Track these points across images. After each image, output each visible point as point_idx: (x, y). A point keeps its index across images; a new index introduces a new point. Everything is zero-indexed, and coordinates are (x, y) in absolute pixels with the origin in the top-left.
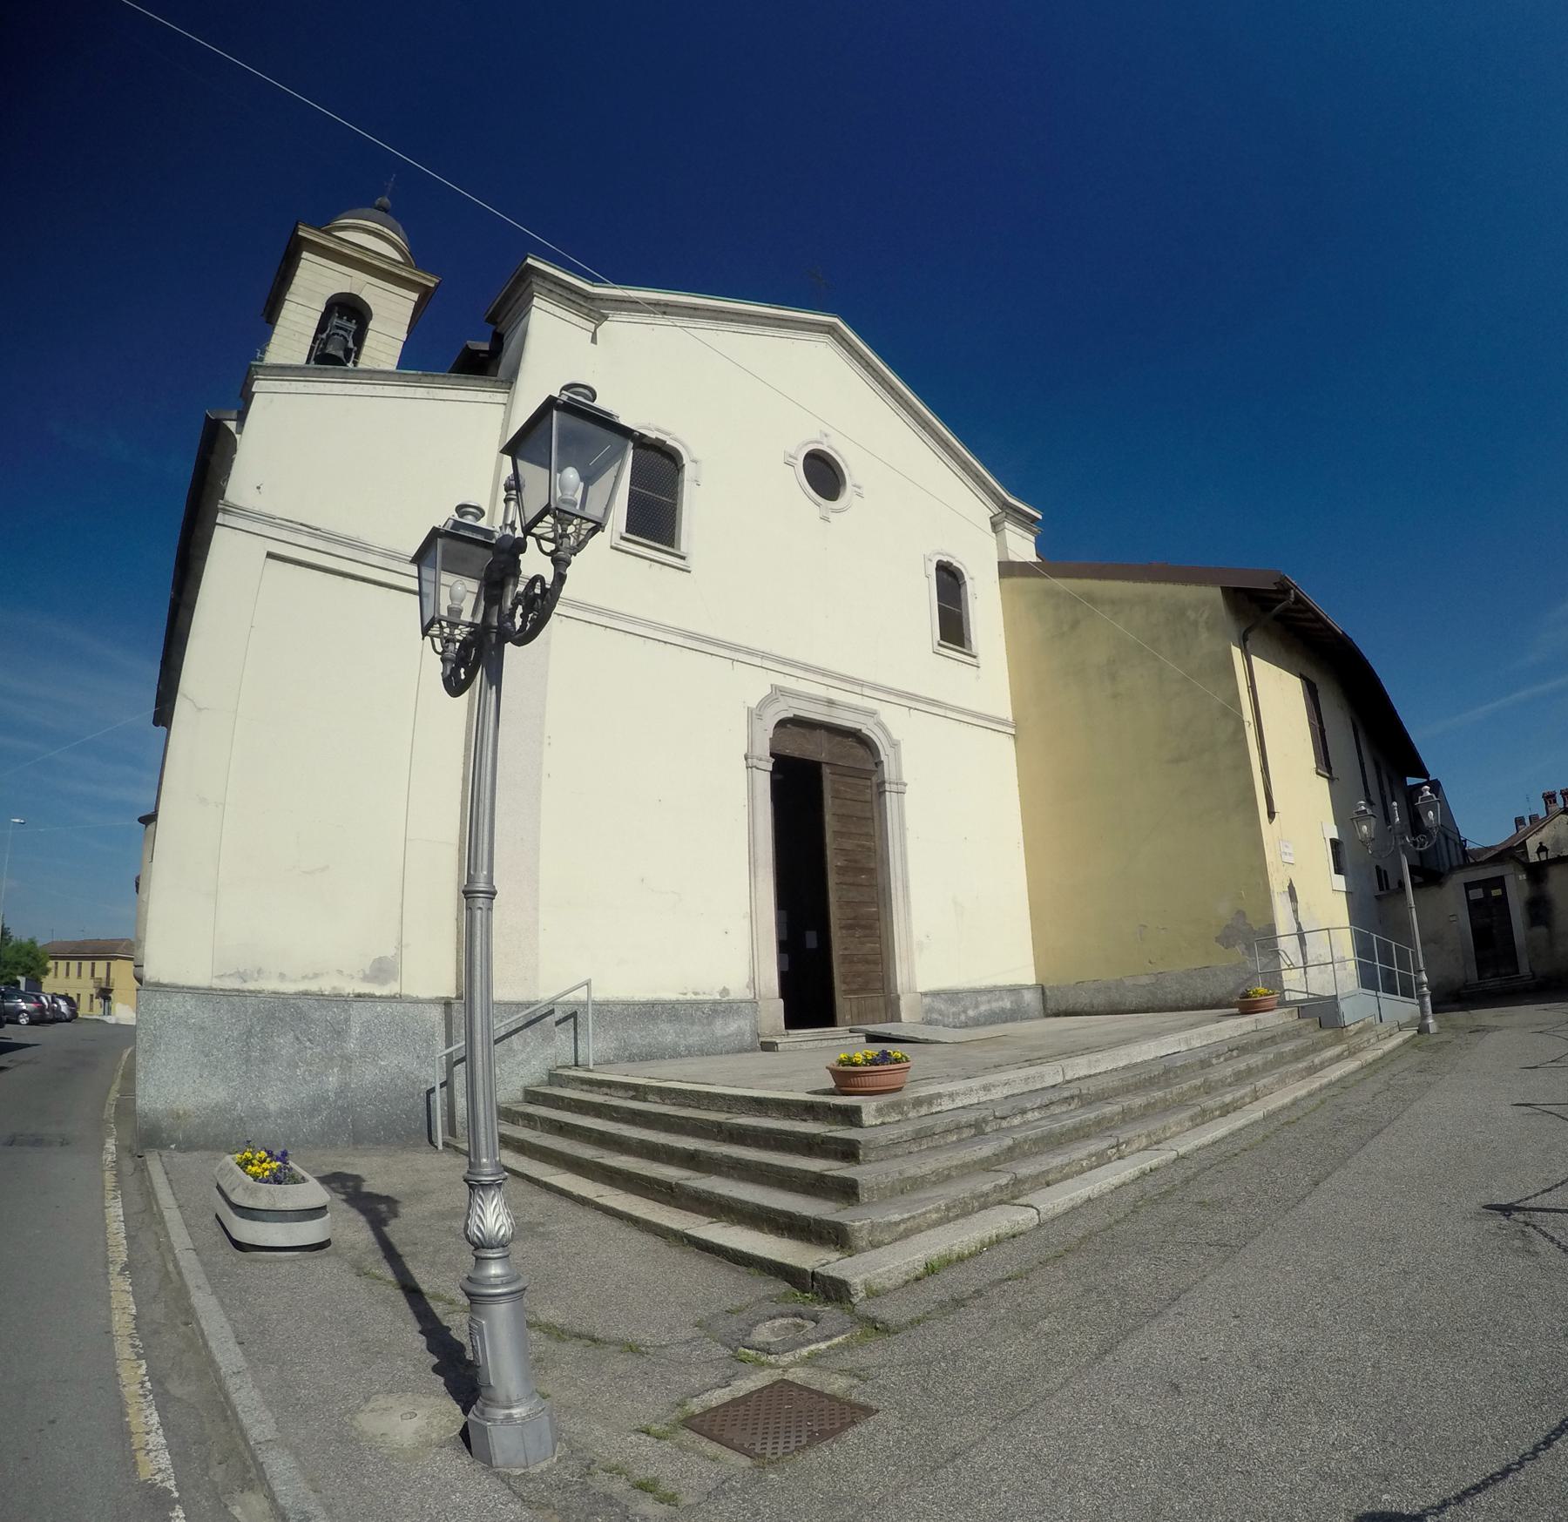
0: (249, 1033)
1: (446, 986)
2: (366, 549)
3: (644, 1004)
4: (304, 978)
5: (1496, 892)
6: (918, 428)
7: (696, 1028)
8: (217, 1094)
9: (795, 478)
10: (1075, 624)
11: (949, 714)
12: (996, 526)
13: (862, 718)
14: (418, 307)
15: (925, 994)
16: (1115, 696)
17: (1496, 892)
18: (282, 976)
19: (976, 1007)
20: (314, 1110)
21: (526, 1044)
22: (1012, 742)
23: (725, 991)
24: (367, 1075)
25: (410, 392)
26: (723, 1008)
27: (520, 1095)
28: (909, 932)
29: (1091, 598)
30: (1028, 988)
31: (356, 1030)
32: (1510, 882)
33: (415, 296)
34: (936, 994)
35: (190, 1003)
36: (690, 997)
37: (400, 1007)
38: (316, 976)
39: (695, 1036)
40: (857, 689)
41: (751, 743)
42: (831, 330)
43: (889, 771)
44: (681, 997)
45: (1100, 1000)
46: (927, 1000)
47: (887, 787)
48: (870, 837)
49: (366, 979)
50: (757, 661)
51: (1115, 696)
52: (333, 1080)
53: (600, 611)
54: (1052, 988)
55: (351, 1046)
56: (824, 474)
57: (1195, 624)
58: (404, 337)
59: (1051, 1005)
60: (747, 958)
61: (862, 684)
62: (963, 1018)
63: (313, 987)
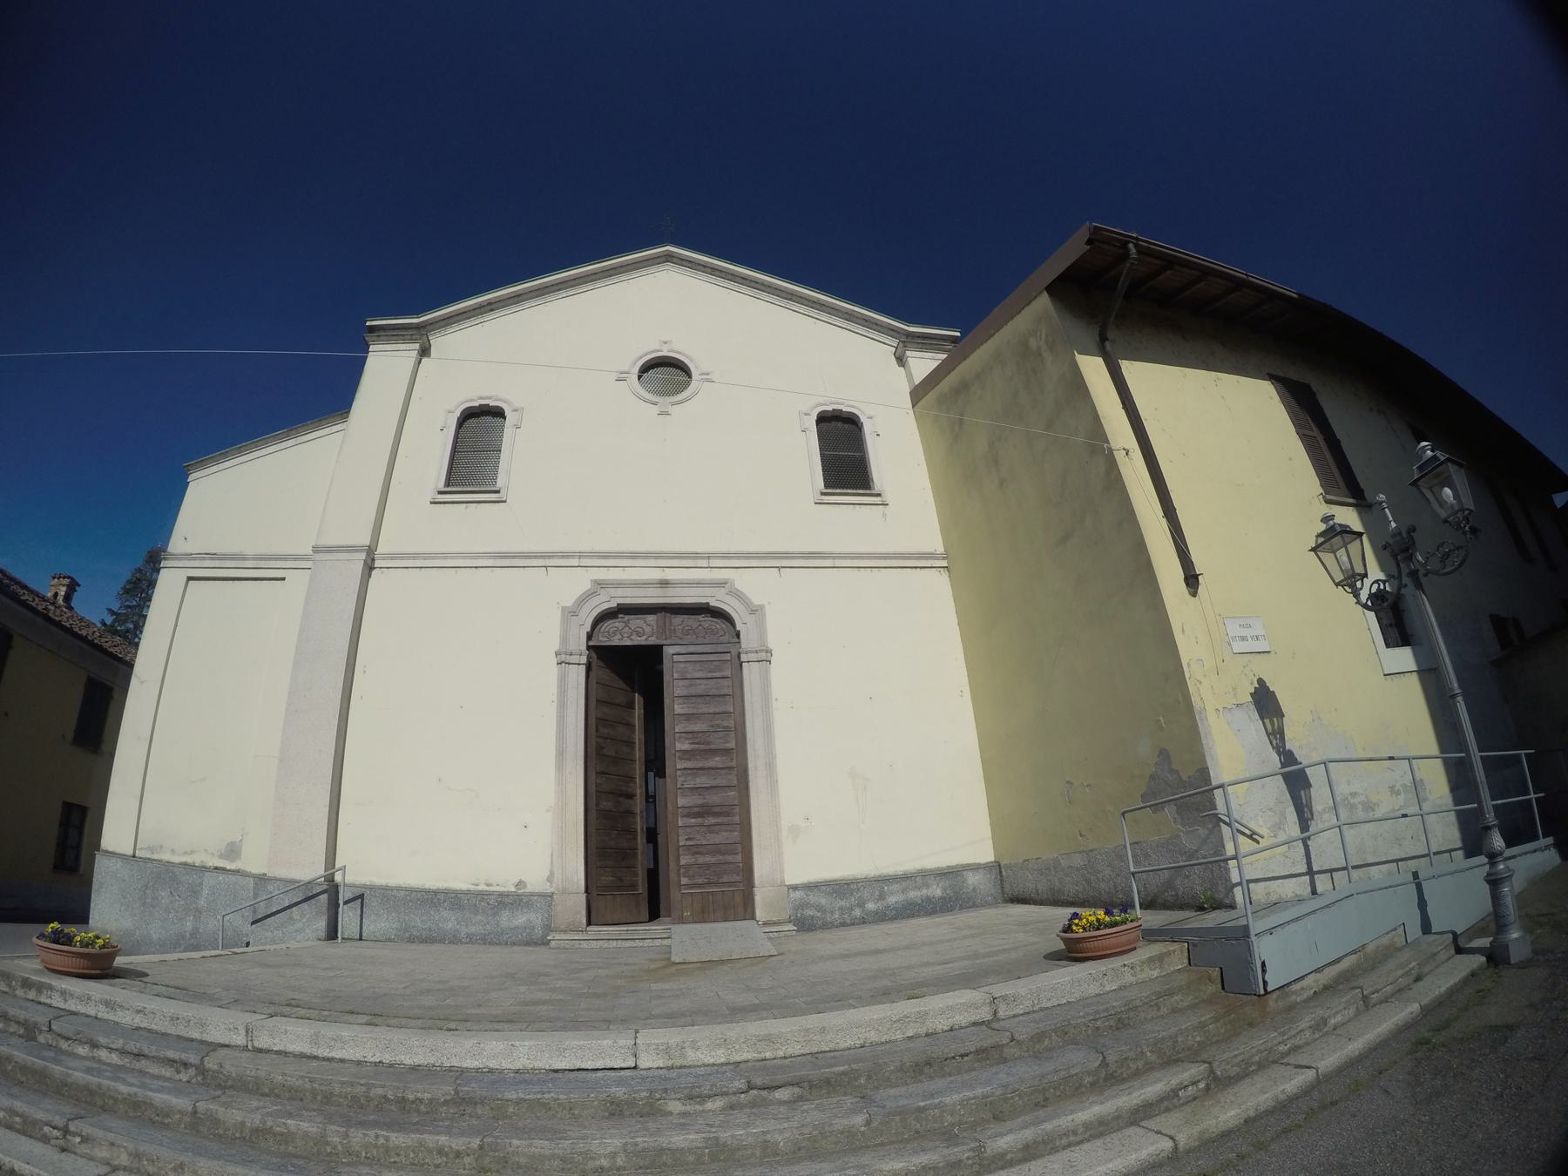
0: (146, 886)
2: (244, 558)
3: (428, 891)
6: (783, 302)
7: (479, 918)
8: (127, 923)
11: (838, 563)
12: (901, 360)
13: (708, 591)
15: (795, 888)
18: (173, 851)
19: (882, 897)
21: (303, 916)
22: (945, 575)
23: (520, 884)
25: (283, 445)
26: (515, 900)
30: (975, 868)
31: (205, 892)
34: (811, 887)
36: (482, 887)
39: (477, 924)
40: (704, 563)
41: (564, 639)
42: (669, 258)
43: (748, 640)
44: (472, 888)
46: (798, 894)
47: (744, 657)
49: (221, 856)
50: (575, 562)
52: (189, 925)
53: (415, 556)
54: (1008, 867)
55: (202, 902)
56: (665, 372)
62: (857, 912)
63: (189, 860)
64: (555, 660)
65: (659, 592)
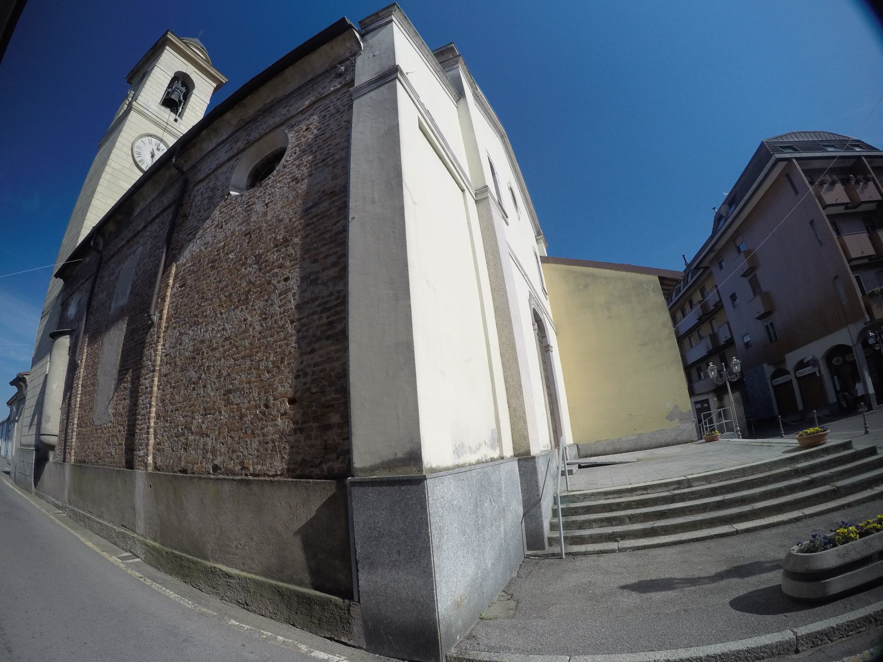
5: (706, 405)
10: (586, 286)
14: (216, 90)
16: (610, 317)
17: (706, 405)
29: (594, 276)
32: (711, 402)
33: (215, 85)
45: (609, 448)
51: (610, 317)
57: (648, 290)
58: (208, 102)
59: (583, 452)
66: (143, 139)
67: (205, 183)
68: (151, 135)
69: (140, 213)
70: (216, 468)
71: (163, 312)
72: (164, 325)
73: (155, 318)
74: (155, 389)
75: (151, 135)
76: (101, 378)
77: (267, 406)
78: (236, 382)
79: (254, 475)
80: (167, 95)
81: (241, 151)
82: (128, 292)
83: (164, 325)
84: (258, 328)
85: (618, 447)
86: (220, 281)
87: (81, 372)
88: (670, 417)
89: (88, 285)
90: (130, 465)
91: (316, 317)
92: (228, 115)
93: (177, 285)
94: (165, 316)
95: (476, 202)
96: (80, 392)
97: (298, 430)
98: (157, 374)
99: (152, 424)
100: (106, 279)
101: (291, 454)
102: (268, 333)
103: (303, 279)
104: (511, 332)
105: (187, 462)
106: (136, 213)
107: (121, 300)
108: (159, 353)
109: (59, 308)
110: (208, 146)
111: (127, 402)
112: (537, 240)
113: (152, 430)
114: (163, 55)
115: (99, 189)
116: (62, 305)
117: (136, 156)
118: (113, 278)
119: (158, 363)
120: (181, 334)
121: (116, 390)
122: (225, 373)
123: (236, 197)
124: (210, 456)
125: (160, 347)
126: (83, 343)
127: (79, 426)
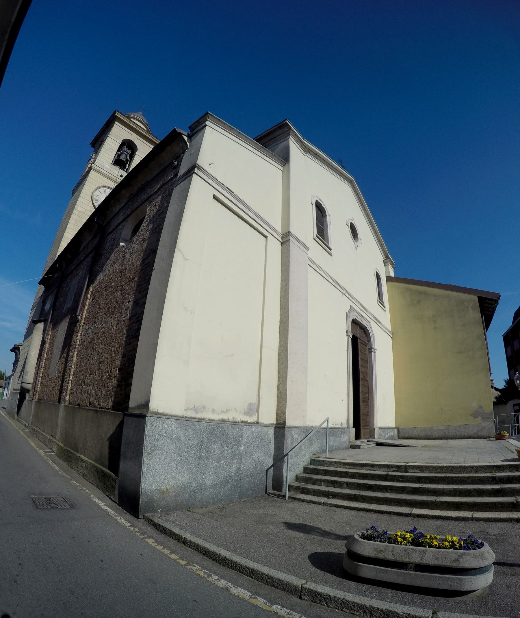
0: (201, 443)
1: (273, 420)
2: (249, 208)
4: (223, 412)
9: (348, 230)
10: (419, 302)
16: (435, 328)
18: (213, 411)
20: (227, 482)
24: (248, 463)
27: (302, 470)
28: (376, 405)
29: (425, 293)
31: (244, 440)
35: (174, 425)
37: (260, 428)
38: (227, 411)
42: (351, 182)
45: (422, 434)
48: (367, 368)
49: (247, 413)
51: (435, 328)
55: (242, 448)
59: (401, 435)
60: (346, 412)
61: (367, 311)
63: (225, 417)
64: (377, 351)
65: (360, 318)
66: (100, 190)
67: (112, 234)
68: (105, 187)
69: (84, 249)
70: (90, 404)
71: (83, 315)
72: (83, 322)
73: (79, 317)
74: (75, 358)
75: (105, 187)
76: (55, 350)
77: (111, 372)
78: (103, 357)
79: (102, 408)
80: (118, 157)
81: (129, 216)
82: (72, 299)
83: (83, 322)
84: (115, 328)
85: (429, 434)
86: (107, 299)
87: (47, 345)
88: (475, 415)
89: (55, 291)
90: (59, 402)
91: (134, 325)
92: (124, 192)
93: (92, 299)
94: (84, 317)
95: (282, 243)
96: (45, 358)
97: (118, 386)
98: (76, 350)
99: (71, 378)
100: (64, 289)
101: (115, 398)
102: (118, 331)
103: (135, 302)
104: (287, 339)
105: (81, 400)
106: (81, 248)
107: (69, 305)
108: (79, 338)
109: (41, 304)
110: (116, 210)
111: (64, 365)
112: (384, 263)
113: (70, 382)
114: (113, 128)
115: (69, 226)
116: (43, 302)
117: (94, 202)
118: (67, 289)
119: (78, 344)
120: (89, 328)
121: (60, 358)
122: (100, 352)
123: (123, 246)
124: (89, 397)
125: (79, 335)
126: (49, 328)
127: (42, 378)
